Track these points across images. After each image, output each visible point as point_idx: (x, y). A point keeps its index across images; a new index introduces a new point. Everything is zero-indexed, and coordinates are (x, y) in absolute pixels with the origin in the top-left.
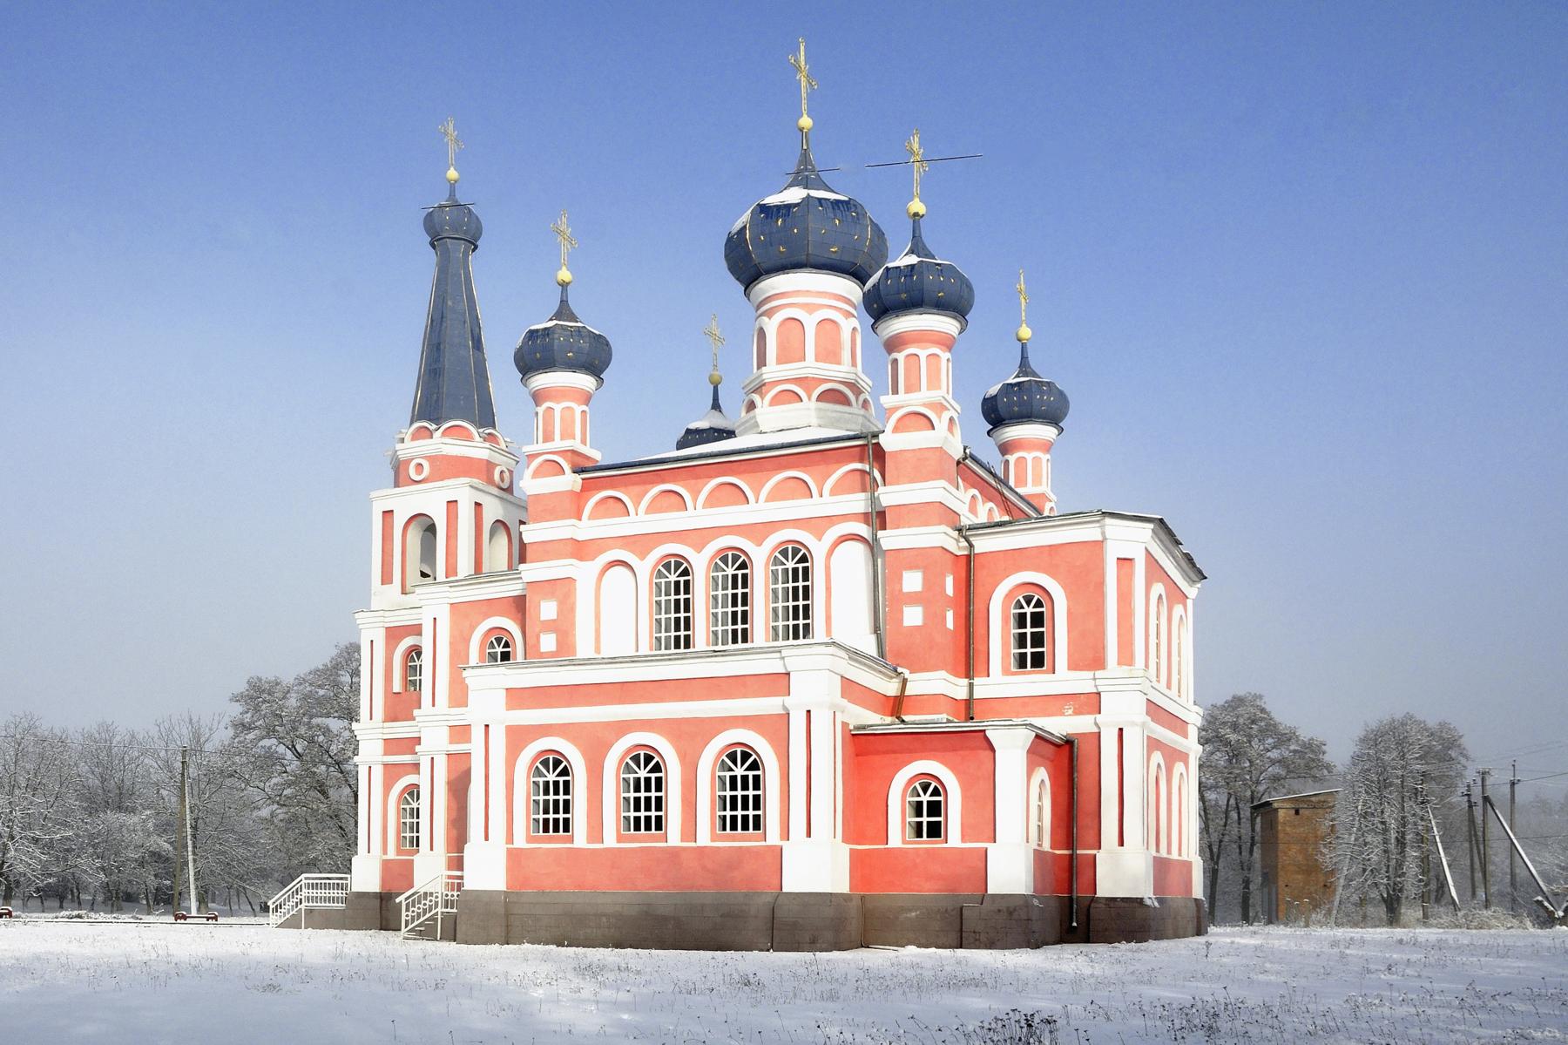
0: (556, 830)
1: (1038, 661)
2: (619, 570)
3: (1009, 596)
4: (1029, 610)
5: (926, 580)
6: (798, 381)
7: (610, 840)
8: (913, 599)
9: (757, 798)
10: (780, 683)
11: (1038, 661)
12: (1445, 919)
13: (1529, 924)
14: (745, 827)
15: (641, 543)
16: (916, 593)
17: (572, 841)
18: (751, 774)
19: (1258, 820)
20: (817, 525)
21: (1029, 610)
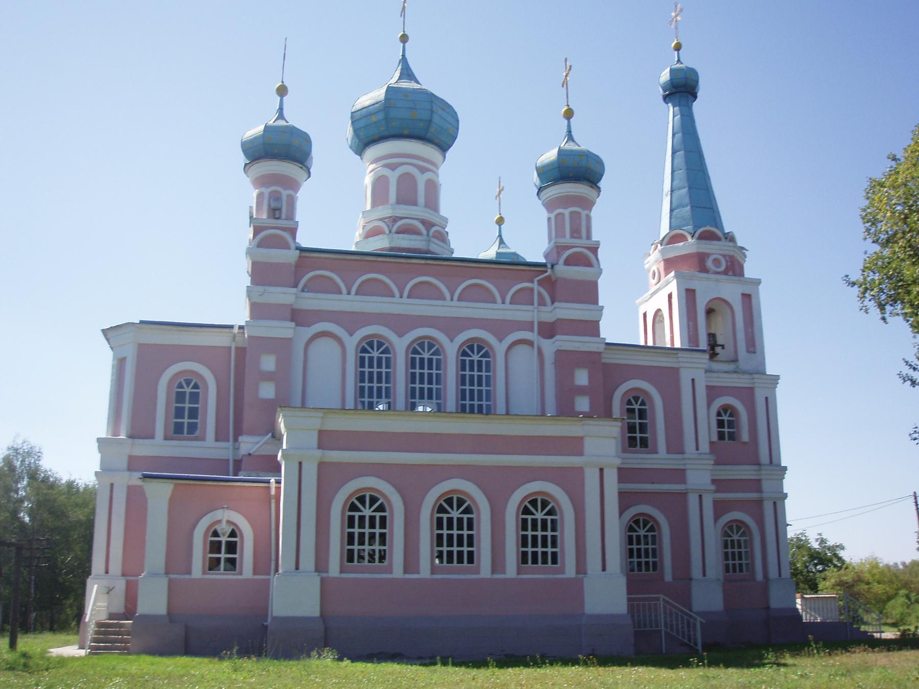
0: (545, 562)
1: (192, 428)
2: (522, 349)
3: (178, 375)
4: (188, 390)
5: (278, 362)
6: (423, 222)
7: (425, 571)
8: (268, 377)
9: (470, 537)
10: (575, 445)
11: (644, 443)
12: (254, 659)
13: (789, 660)
14: (545, 562)
15: (351, 321)
16: (270, 372)
17: (478, 572)
18: (378, 514)
19: (759, 576)
20: (501, 328)
21: (188, 390)
